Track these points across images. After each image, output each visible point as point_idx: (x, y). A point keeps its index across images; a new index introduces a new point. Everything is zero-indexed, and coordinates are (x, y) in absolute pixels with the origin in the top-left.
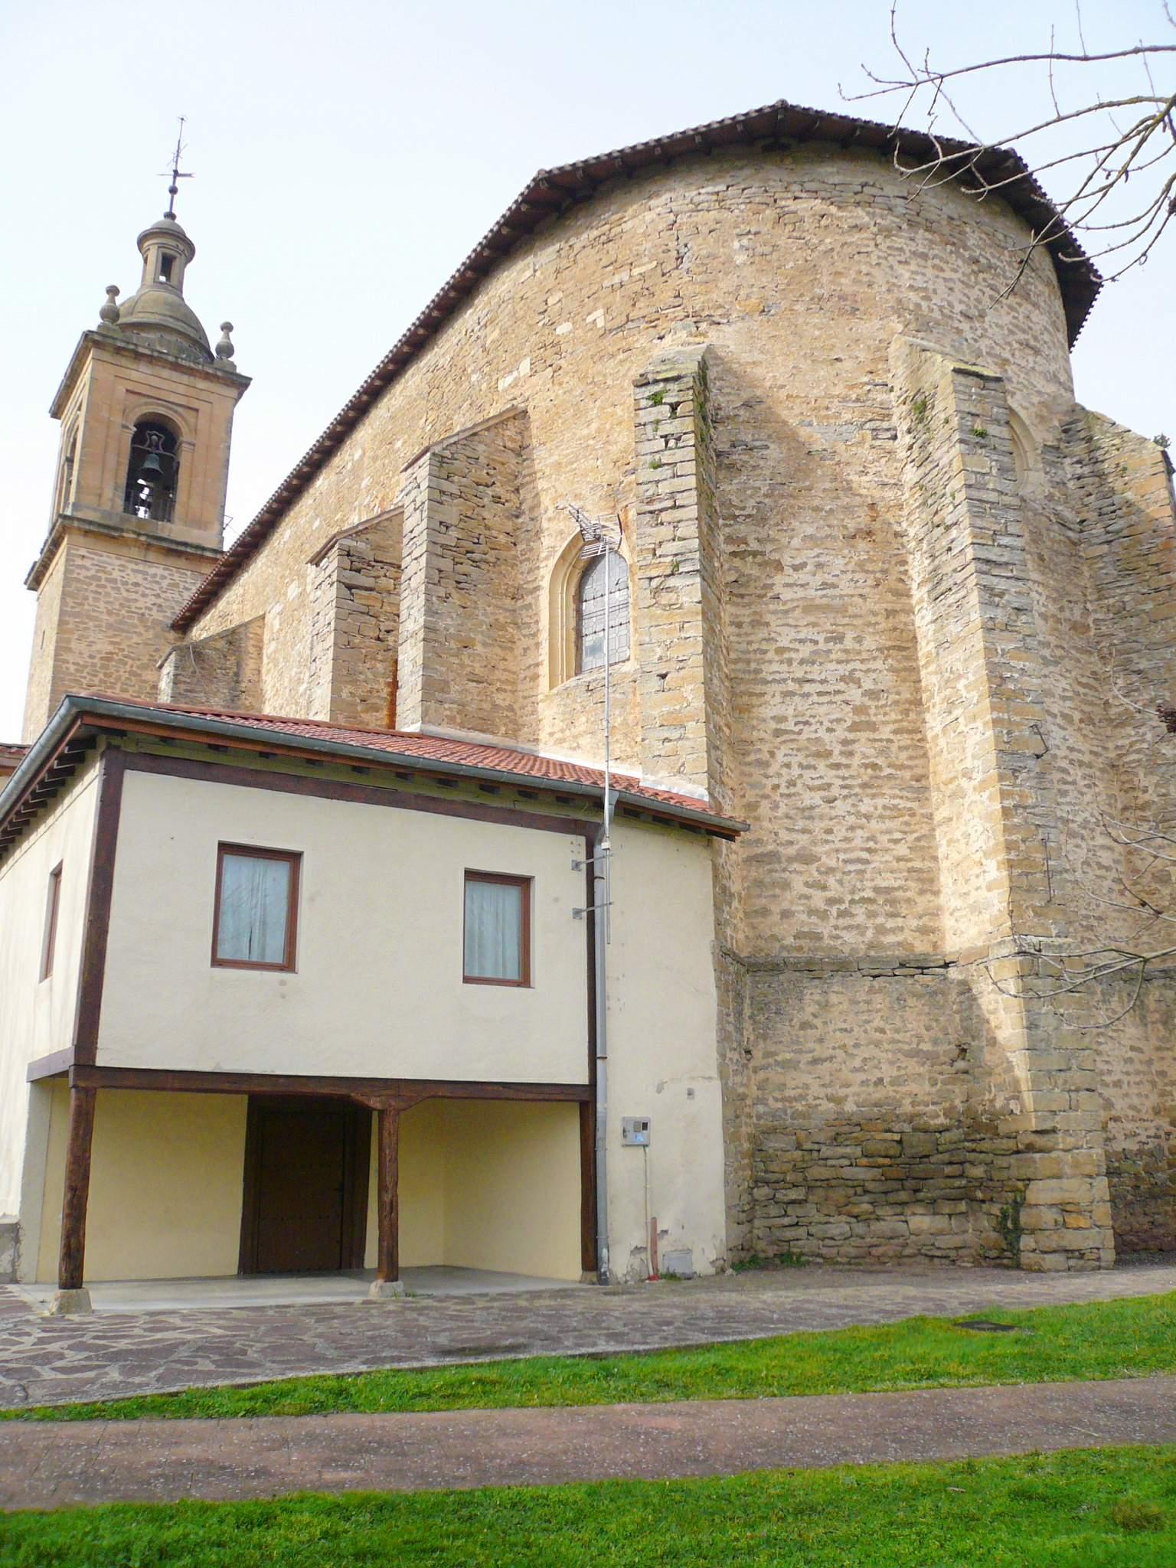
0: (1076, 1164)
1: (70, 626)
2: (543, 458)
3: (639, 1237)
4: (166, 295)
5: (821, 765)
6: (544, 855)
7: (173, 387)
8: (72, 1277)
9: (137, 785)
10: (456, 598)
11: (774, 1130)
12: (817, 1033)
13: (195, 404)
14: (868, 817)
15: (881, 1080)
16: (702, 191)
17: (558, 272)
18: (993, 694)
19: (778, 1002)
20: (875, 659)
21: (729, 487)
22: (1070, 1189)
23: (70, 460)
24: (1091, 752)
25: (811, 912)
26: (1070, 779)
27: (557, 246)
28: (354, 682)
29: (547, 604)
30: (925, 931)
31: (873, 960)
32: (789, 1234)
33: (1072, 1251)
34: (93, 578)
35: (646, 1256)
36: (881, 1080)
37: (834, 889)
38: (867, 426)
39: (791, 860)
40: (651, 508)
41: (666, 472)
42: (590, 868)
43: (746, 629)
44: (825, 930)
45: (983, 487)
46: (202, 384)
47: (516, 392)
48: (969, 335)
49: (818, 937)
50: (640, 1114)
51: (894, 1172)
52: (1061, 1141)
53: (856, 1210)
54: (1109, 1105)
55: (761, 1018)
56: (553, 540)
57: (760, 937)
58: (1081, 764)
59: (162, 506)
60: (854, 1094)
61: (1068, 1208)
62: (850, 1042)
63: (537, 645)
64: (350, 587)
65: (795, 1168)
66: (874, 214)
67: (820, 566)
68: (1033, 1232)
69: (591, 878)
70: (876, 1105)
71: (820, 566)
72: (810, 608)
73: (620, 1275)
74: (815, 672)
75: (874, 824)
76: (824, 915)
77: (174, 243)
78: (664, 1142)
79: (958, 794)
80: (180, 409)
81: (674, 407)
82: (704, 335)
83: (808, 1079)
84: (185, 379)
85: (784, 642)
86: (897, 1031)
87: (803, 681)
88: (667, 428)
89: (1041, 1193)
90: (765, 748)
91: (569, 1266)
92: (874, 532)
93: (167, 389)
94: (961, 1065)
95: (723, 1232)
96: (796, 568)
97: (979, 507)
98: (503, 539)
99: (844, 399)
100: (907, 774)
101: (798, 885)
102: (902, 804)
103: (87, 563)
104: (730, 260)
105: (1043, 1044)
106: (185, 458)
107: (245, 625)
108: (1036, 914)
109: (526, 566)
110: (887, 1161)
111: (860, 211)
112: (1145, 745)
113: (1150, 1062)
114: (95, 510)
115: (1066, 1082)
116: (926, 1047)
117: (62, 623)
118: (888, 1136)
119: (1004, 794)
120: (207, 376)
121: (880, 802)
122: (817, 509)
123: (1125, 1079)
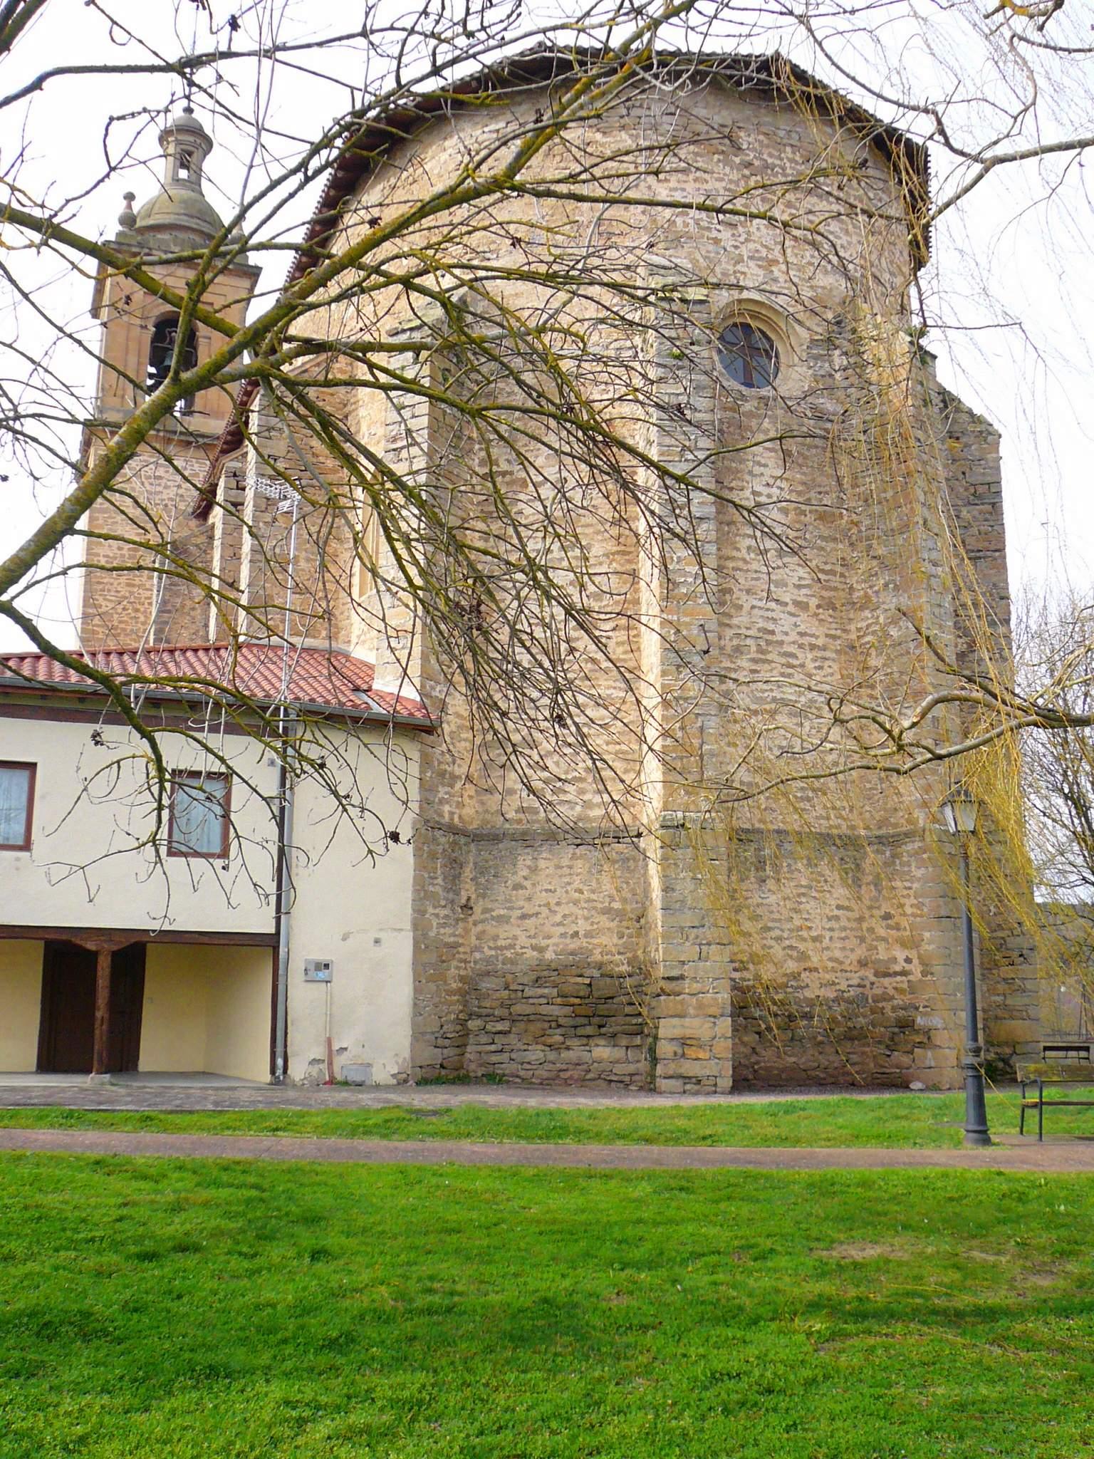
0: (700, 1006)
1: (100, 522)
3: (318, 1052)
4: (183, 192)
11: (488, 973)
12: (527, 893)
15: (576, 933)
16: (486, 129)
19: (496, 867)
20: (601, 564)
24: (827, 636)
26: (795, 662)
27: (381, 186)
32: (494, 1058)
33: (689, 1078)
35: (324, 1066)
36: (576, 933)
38: (612, 346)
40: (394, 446)
48: (729, 244)
50: (323, 958)
52: (687, 985)
53: (549, 1041)
55: (482, 880)
57: (487, 811)
58: (813, 647)
60: (555, 945)
61: (688, 1042)
62: (553, 902)
65: (502, 1005)
66: (637, 136)
70: (572, 954)
73: (297, 1079)
77: (192, 139)
78: (347, 983)
83: (518, 932)
86: (593, 892)
89: (668, 1028)
95: (406, 1053)
105: (678, 905)
108: (687, 793)
110: (577, 1001)
111: (624, 135)
112: (877, 628)
114: (118, 411)
115: (697, 937)
116: (616, 905)
118: (579, 980)
123: (828, 934)
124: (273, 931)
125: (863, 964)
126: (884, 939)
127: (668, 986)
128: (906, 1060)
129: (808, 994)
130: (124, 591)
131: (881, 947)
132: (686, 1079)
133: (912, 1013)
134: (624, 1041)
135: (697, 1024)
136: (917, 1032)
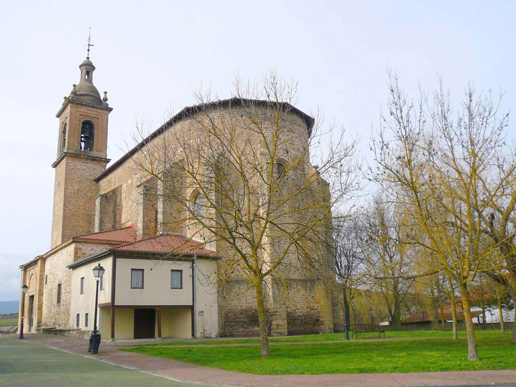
3: (202, 331)
6: (185, 266)
8: (113, 336)
9: (118, 260)
10: (169, 204)
13: (98, 117)
23: (64, 132)
28: (147, 217)
32: (232, 331)
46: (99, 111)
50: (202, 310)
52: (278, 313)
59: (89, 145)
69: (193, 269)
77: (90, 67)
80: (94, 119)
84: (95, 110)
89: (274, 323)
91: (190, 336)
93: (91, 113)
103: (71, 164)
106: (95, 132)
107: (117, 188)
113: (307, 298)
117: (66, 181)
120: (101, 109)
125: (307, 307)
127: (274, 314)
128: (318, 328)
129: (298, 314)
130: (75, 203)
131: (311, 304)
132: (278, 333)
135: (280, 322)
136: (320, 322)
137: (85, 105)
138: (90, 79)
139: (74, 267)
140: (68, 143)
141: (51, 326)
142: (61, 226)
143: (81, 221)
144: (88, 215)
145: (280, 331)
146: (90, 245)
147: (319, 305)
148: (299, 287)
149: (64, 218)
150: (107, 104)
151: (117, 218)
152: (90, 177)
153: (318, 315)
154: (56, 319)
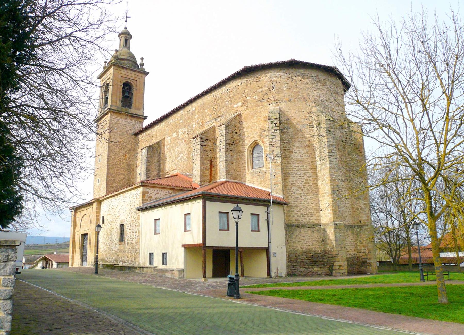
2: (245, 125)
3: (275, 271)
5: (300, 190)
6: (261, 210)
7: (131, 75)
9: (208, 203)
10: (230, 154)
11: (292, 253)
13: (136, 79)
14: (307, 199)
17: (247, 85)
18: (331, 180)
21: (283, 137)
22: (341, 264)
25: (298, 216)
27: (246, 80)
28: (204, 165)
29: (247, 155)
30: (317, 219)
31: (308, 225)
32: (294, 271)
34: (116, 123)
37: (302, 212)
39: (294, 207)
41: (274, 137)
42: (268, 213)
43: (286, 164)
44: (300, 219)
45: (330, 141)
46: (138, 74)
47: (238, 109)
49: (299, 220)
50: (275, 251)
51: (312, 260)
54: (347, 249)
56: (248, 142)
59: (130, 106)
63: (245, 163)
64: (202, 145)
67: (300, 152)
68: (335, 270)
71: (300, 152)
72: (298, 160)
74: (299, 173)
75: (309, 201)
76: (300, 217)
79: (324, 196)
81: (275, 124)
82: (278, 105)
84: (134, 73)
85: (293, 167)
87: (296, 174)
88: (275, 128)
89: (336, 264)
90: (290, 186)
91: (265, 275)
92: (310, 146)
93: (130, 75)
94: (323, 243)
96: (295, 153)
97: (329, 145)
98: (237, 141)
99: (304, 119)
100: (314, 192)
101: (296, 211)
102: (314, 197)
103: (114, 119)
104: (283, 89)
106: (134, 92)
109: (242, 147)
111: (307, 80)
116: (317, 239)
119: (332, 198)
121: (310, 196)
122: (299, 141)
124: (267, 246)
125: (355, 250)
126: (359, 246)
130: (117, 153)
131: (359, 247)
133: (366, 260)
134: (320, 266)
135: (341, 264)
137: (126, 68)
138: (128, 46)
139: (142, 210)
140: (112, 101)
141: (111, 261)
142: (106, 174)
143: (122, 170)
144: (128, 165)
145: (341, 271)
146: (156, 189)
147: (366, 248)
148: (348, 232)
149: (108, 166)
150: (144, 69)
151: (161, 167)
152: (130, 132)
153: (365, 257)
154: (118, 255)
